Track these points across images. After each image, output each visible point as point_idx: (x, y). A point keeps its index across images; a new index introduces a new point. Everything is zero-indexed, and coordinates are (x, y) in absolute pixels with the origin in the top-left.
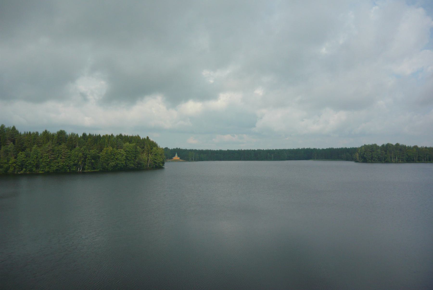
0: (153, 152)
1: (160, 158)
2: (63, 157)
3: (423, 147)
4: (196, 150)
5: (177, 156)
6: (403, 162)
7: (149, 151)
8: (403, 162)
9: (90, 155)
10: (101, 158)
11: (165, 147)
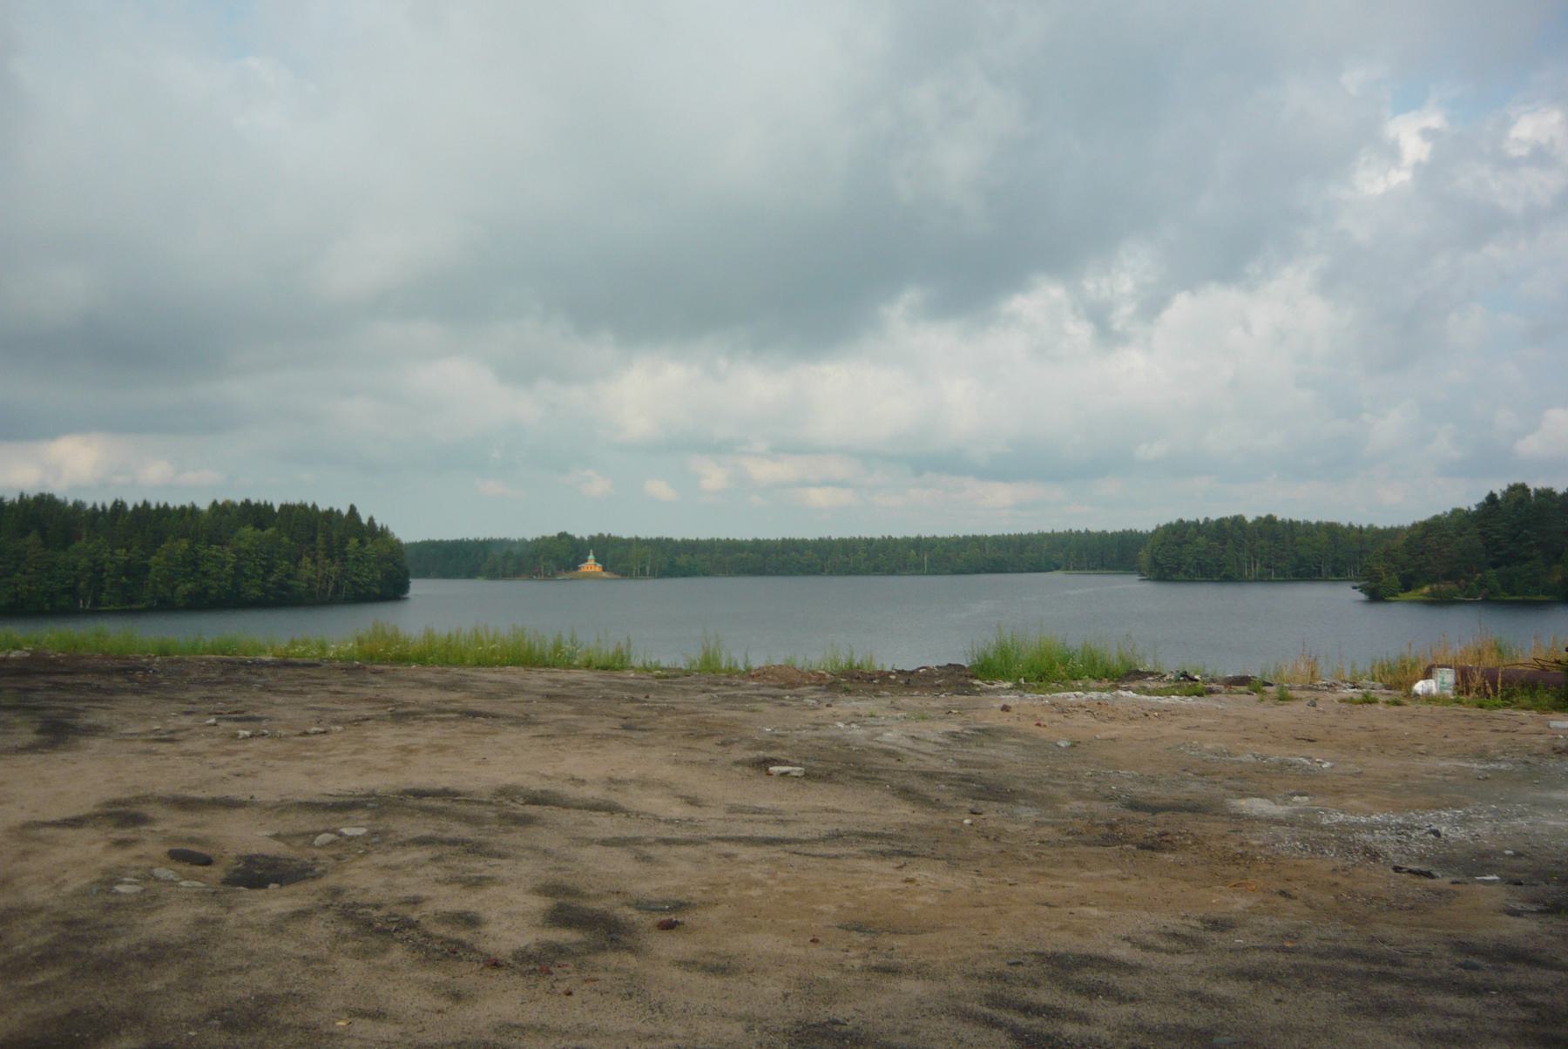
2: (31, 570)
3: (1147, 531)
5: (593, 562)
6: (1281, 579)
8: (1281, 579)
9: (114, 565)
10: (153, 570)
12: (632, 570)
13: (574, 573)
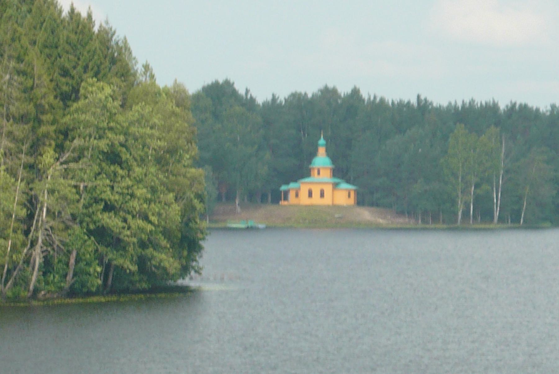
0: (87, 125)
1: (153, 190)
4: (524, 108)
5: (326, 176)
7: (44, 118)
11: (209, 81)
12: (454, 203)
13: (271, 208)
